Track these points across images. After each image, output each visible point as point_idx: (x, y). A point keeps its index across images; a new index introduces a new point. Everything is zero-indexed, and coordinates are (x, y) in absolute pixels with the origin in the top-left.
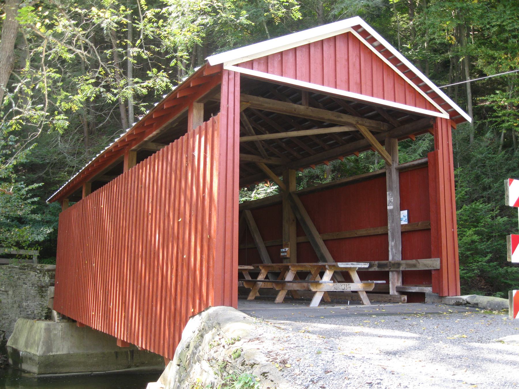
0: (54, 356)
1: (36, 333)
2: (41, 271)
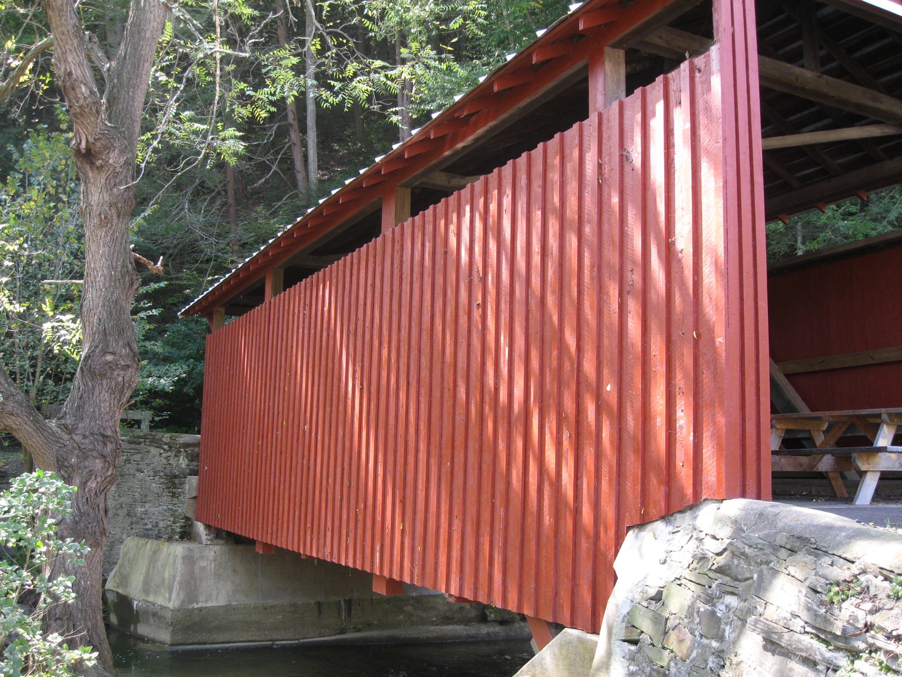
0: (200, 609)
1: (164, 566)
2: (170, 447)
